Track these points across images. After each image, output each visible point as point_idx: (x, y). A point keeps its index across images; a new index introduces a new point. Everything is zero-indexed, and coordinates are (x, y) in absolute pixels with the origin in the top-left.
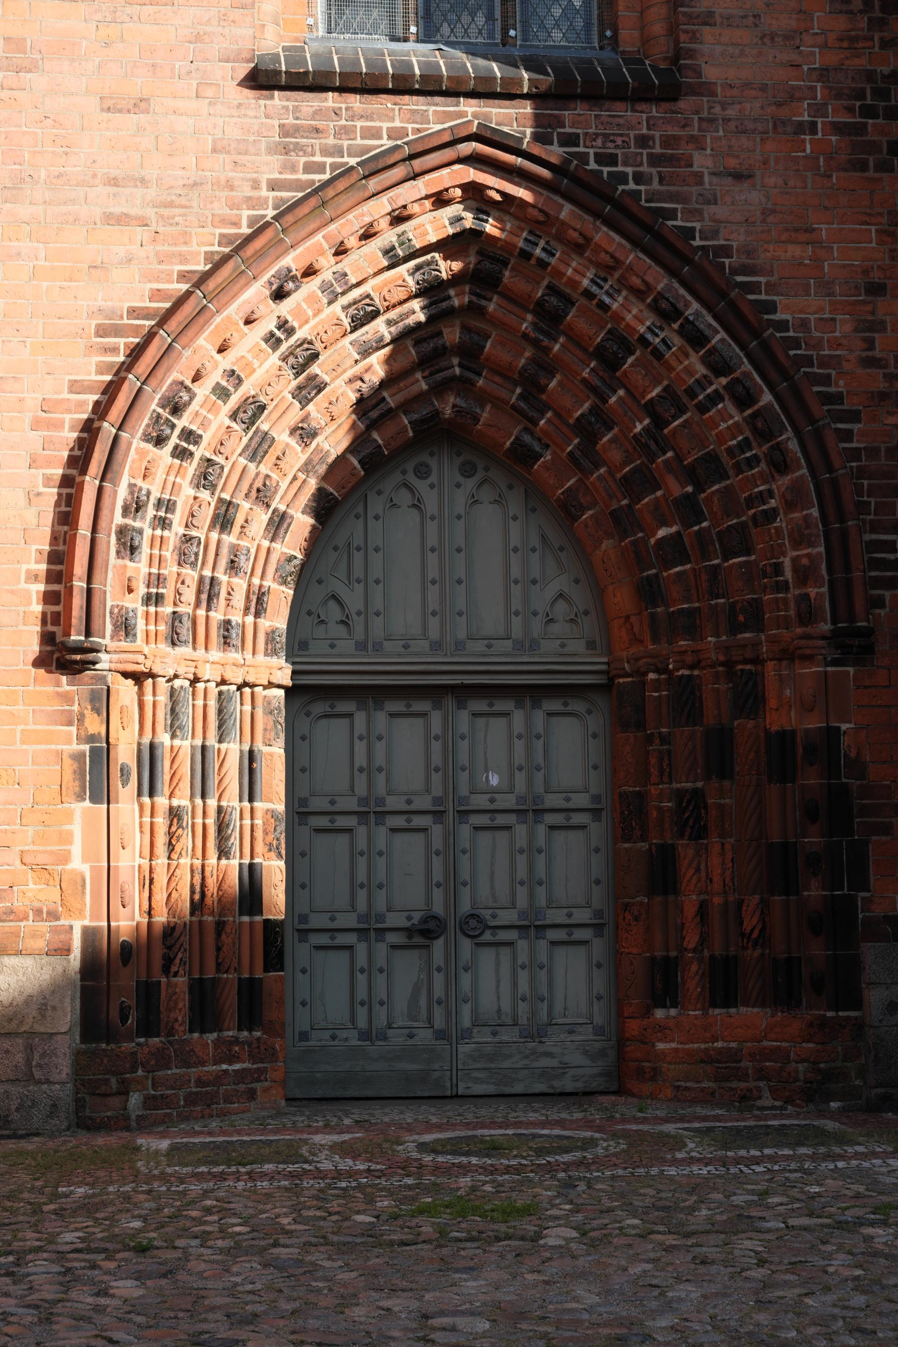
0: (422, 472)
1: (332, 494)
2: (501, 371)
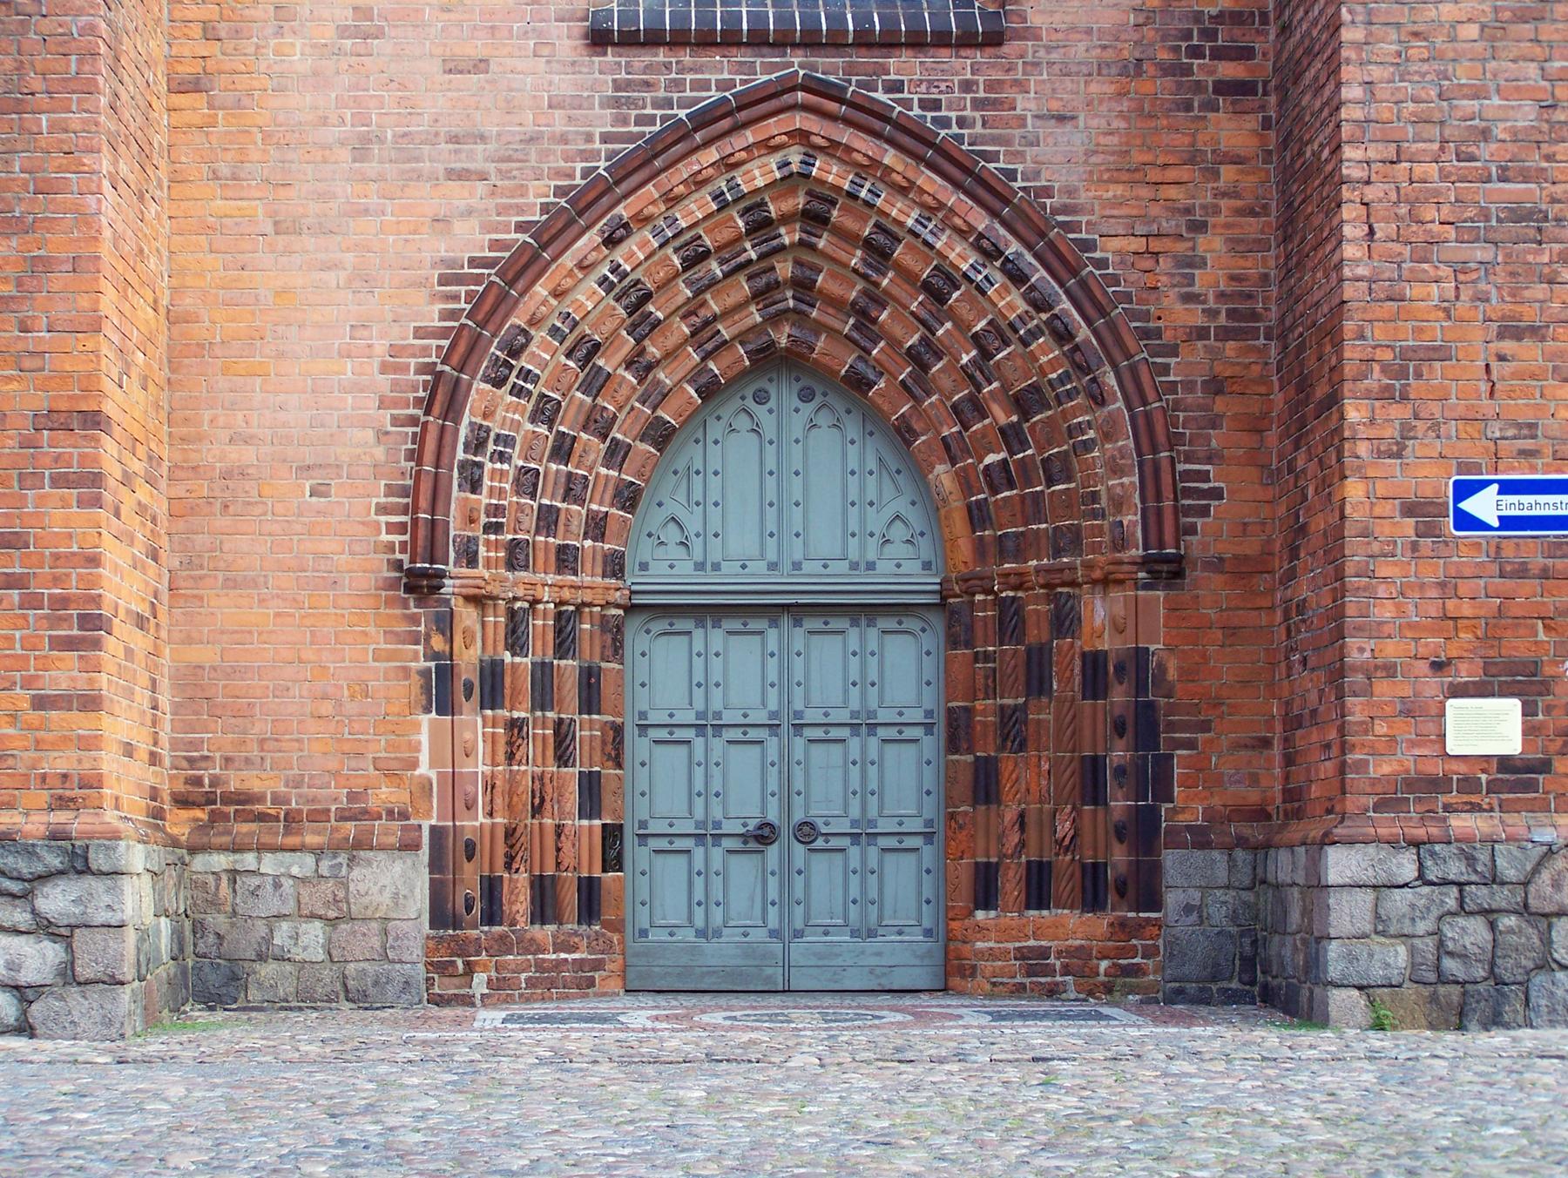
0: (761, 398)
2: (836, 303)
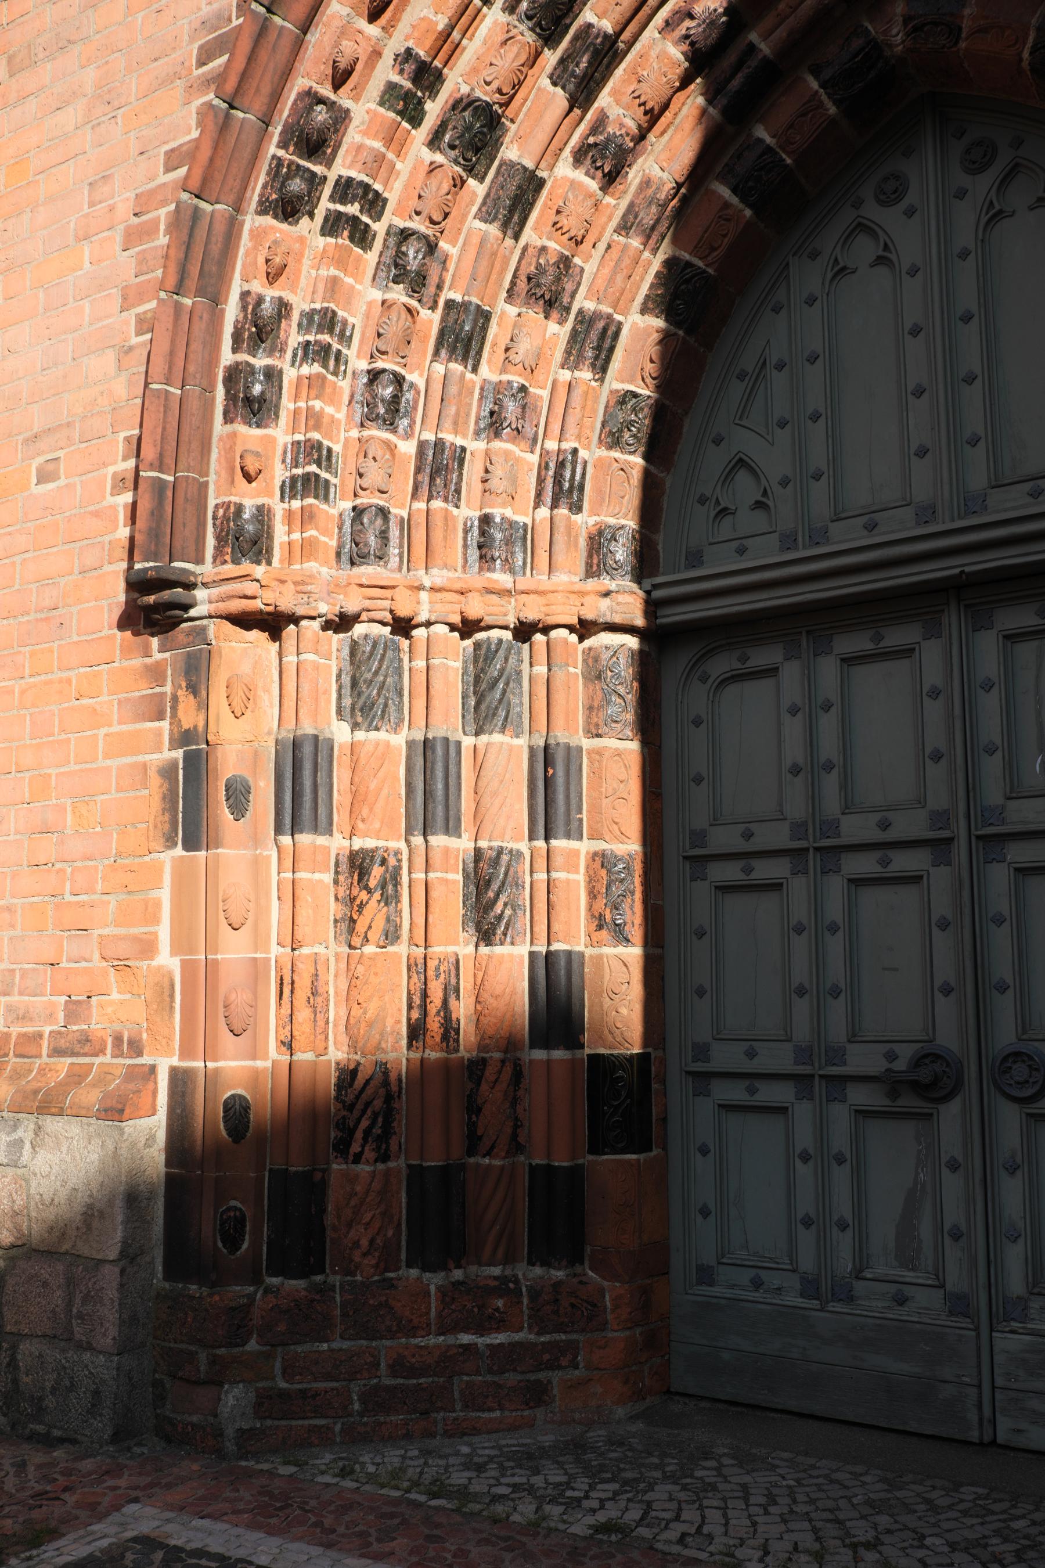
0: (891, 194)
1: (688, 264)
